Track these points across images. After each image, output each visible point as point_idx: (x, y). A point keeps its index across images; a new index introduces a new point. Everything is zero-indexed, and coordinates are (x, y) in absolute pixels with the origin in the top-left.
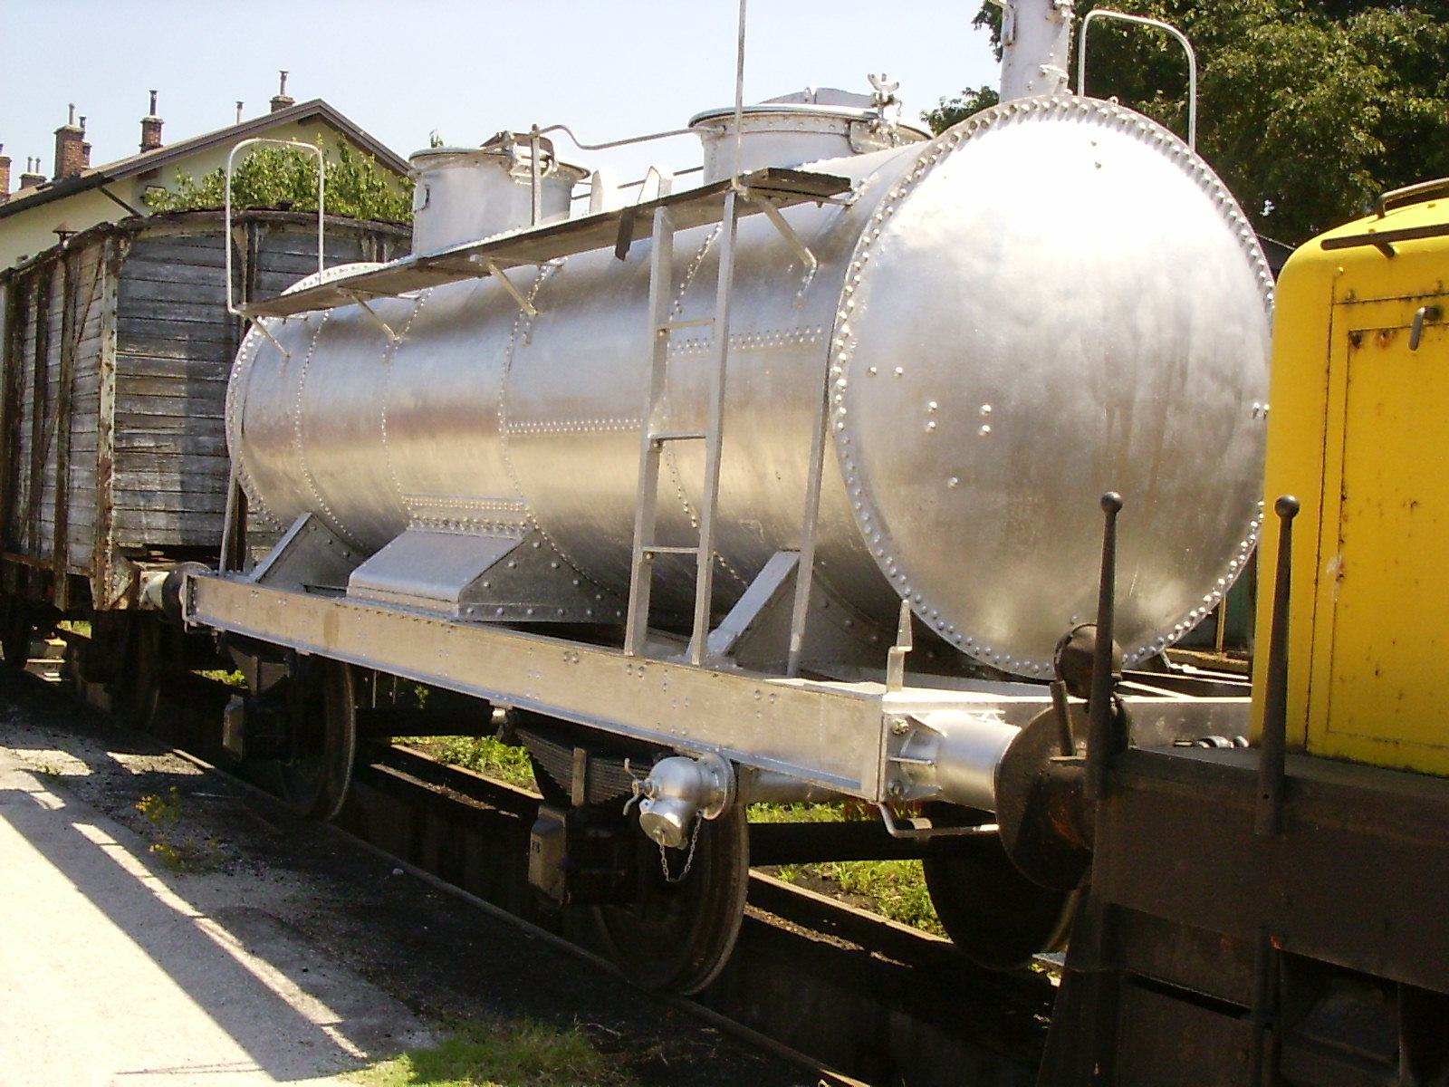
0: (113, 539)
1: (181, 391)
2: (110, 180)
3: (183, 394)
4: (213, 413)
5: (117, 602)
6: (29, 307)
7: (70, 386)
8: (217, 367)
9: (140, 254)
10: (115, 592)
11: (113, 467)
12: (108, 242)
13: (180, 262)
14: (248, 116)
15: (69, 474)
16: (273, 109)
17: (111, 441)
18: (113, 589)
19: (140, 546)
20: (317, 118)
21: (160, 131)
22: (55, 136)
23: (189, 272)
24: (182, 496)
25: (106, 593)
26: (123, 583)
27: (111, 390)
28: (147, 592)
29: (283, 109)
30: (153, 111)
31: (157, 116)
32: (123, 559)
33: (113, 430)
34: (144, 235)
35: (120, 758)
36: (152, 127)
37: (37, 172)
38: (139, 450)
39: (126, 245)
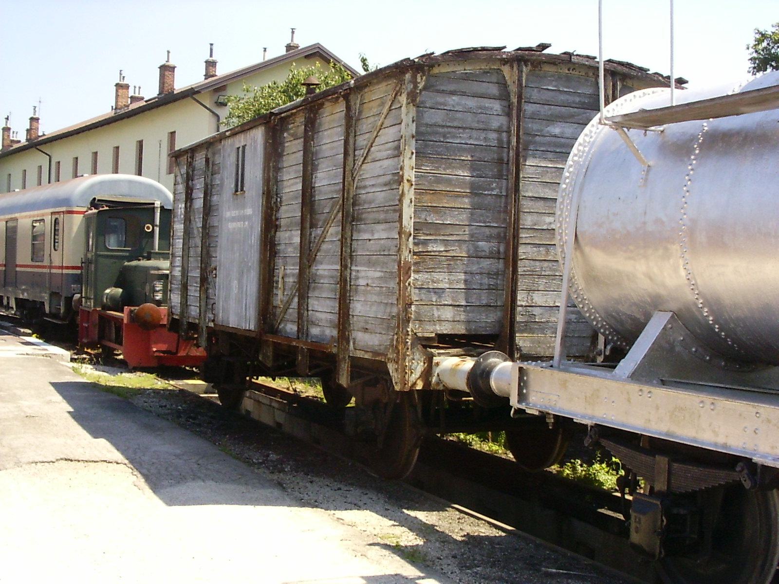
0: (412, 331)
1: (465, 203)
2: (198, 92)
3: (466, 206)
4: (488, 222)
5: (415, 384)
6: (284, 143)
7: (352, 201)
8: (492, 183)
9: (433, 86)
10: (413, 375)
11: (412, 268)
12: (408, 76)
13: (463, 94)
14: (270, 55)
15: (350, 274)
16: (287, 51)
17: (411, 246)
18: (412, 373)
19: (433, 335)
20: (318, 54)
21: (215, 67)
22: (159, 69)
23: (471, 103)
24: (465, 292)
25: (407, 377)
26: (419, 367)
27: (411, 202)
28: (438, 374)
29: (293, 51)
30: (211, 56)
31: (214, 58)
32: (419, 346)
33: (412, 237)
34: (436, 70)
35: (413, 513)
36: (211, 64)
37: (139, 94)
38: (432, 254)
39: (422, 79)
